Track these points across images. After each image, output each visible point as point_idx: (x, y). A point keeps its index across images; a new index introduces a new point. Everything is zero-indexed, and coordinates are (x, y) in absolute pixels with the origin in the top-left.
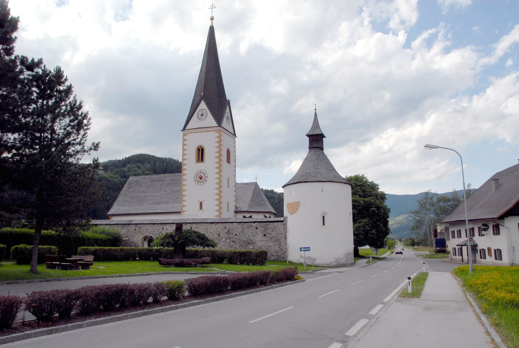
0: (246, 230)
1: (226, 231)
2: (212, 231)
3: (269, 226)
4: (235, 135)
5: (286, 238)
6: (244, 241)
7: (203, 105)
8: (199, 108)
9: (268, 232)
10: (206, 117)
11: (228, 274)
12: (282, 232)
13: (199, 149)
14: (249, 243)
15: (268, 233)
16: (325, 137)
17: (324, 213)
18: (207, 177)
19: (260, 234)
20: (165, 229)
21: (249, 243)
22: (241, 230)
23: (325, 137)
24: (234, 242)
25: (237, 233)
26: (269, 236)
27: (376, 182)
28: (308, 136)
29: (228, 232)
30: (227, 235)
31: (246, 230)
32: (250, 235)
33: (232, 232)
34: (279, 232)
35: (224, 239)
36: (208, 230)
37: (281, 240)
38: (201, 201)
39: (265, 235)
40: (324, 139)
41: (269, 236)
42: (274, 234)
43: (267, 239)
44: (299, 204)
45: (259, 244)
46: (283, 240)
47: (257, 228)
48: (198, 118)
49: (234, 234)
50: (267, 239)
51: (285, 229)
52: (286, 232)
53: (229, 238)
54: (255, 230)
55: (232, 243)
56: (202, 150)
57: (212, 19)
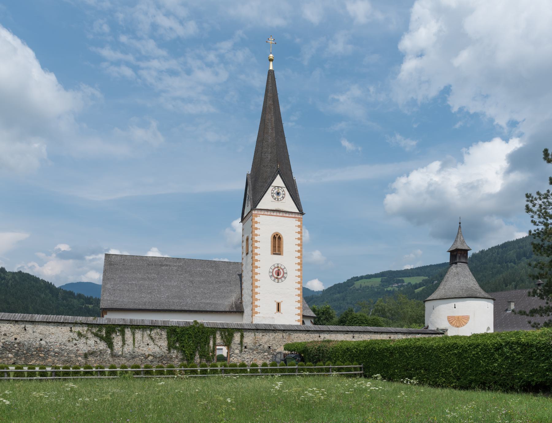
10: (283, 197)
13: (274, 237)
38: (279, 301)
48: (273, 196)
56: (280, 238)
57: (460, 223)
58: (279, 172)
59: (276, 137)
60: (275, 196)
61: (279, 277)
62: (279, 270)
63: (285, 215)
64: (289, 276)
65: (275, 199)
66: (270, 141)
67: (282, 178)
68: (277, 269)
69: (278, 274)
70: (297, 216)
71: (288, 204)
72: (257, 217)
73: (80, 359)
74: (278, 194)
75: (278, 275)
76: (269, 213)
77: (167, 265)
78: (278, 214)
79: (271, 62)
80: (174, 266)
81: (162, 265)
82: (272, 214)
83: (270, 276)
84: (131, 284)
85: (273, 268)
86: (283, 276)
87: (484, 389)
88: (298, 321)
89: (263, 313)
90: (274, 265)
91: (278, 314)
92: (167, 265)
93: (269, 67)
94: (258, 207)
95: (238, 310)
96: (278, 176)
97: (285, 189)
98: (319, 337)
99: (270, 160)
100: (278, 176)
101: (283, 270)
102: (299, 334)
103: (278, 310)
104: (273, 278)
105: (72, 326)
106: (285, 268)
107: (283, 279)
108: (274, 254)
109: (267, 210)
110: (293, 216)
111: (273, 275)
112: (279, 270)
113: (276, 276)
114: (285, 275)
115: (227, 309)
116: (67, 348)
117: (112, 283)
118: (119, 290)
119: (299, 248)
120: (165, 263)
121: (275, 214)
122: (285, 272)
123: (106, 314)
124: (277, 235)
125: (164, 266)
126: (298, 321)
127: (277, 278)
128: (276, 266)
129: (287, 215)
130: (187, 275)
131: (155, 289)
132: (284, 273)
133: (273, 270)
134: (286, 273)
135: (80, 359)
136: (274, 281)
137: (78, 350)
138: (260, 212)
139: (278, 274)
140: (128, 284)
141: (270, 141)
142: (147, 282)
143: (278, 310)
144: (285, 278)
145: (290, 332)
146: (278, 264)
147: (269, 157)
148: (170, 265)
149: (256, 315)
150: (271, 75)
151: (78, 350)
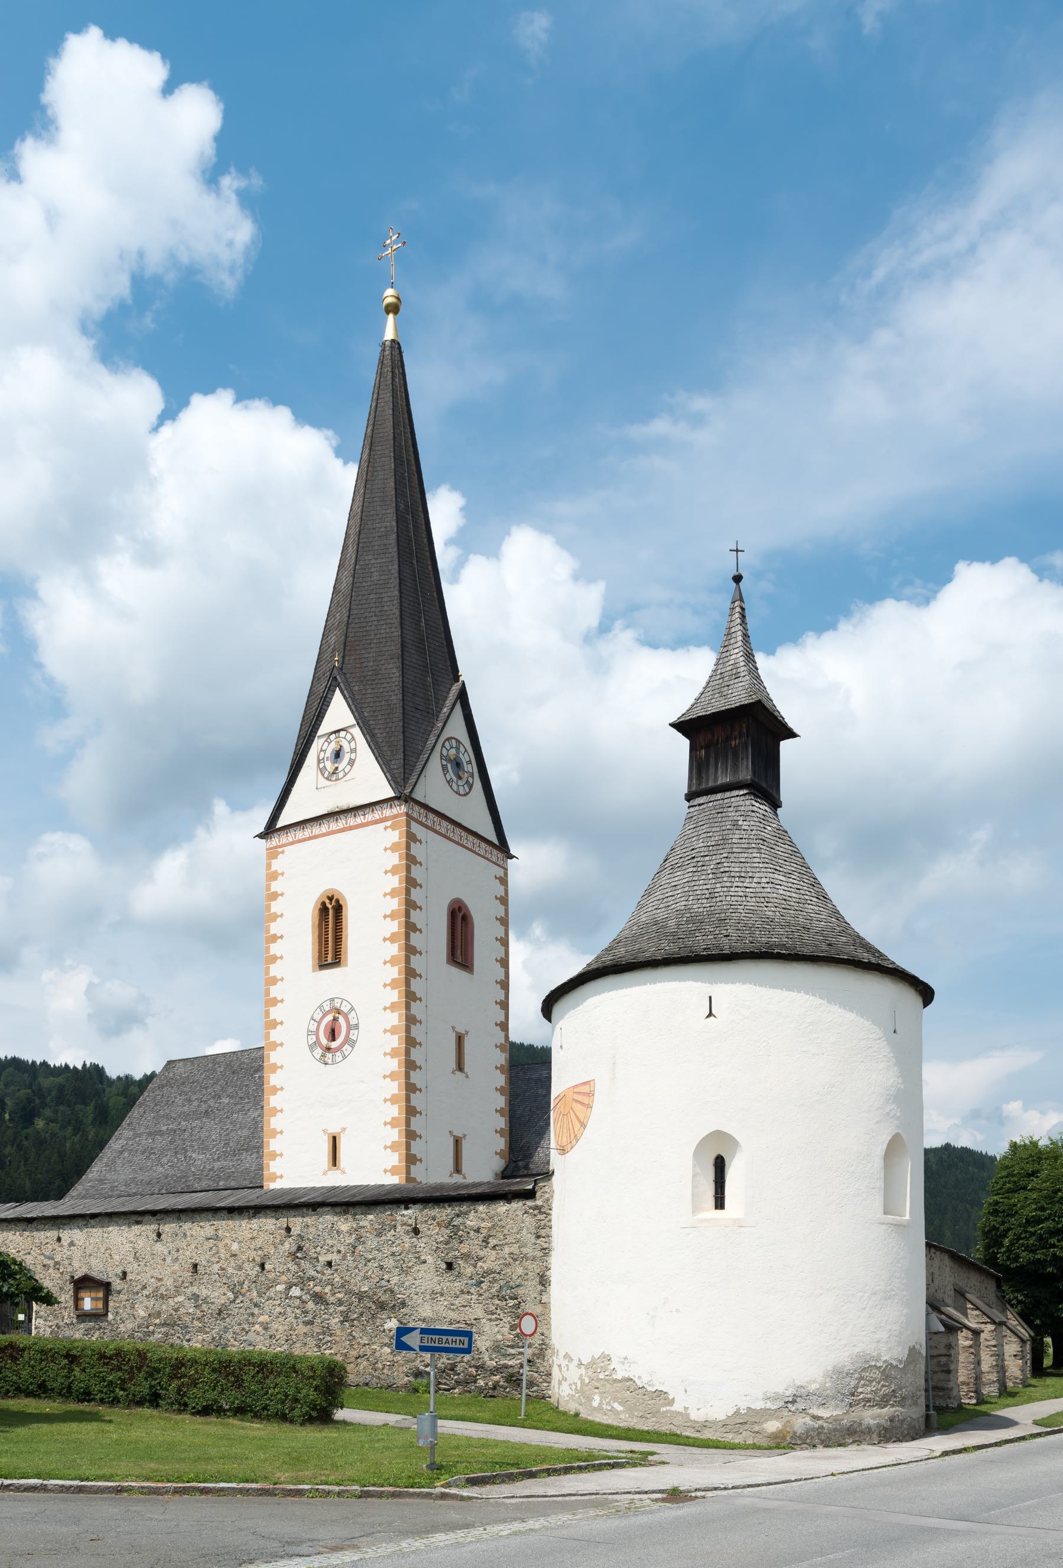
0: (372, 1242)
1: (289, 1245)
2: (235, 1247)
3: (472, 1221)
4: (502, 847)
5: (544, 1281)
6: (361, 1296)
7: (339, 712)
8: (325, 727)
9: (464, 1248)
10: (352, 762)
11: (826, 1420)
12: (528, 1251)
13: (323, 910)
14: (382, 1306)
15: (466, 1257)
16: (791, 734)
17: (719, 1136)
18: (357, 1026)
19: (430, 1259)
20: (65, 1242)
21: (382, 1306)
22: (351, 1240)
23: (791, 734)
24: (319, 1298)
25: (334, 1257)
26: (469, 1270)
27: (783, 804)
28: (682, 726)
29: (298, 1253)
30: (294, 1268)
31: (372, 1242)
32: (389, 1263)
33: (312, 1253)
34: (515, 1249)
35: (280, 1288)
36: (221, 1245)
37: (521, 1295)
38: (334, 1129)
39: (450, 1266)
40: (785, 746)
41: (469, 1270)
42: (491, 1260)
43: (458, 1285)
44: (590, 1094)
45: (426, 1311)
46: (529, 1290)
47: (416, 1231)
48: (322, 771)
49: (323, 1259)
50: (458, 1285)
51: (543, 1232)
52: (546, 1251)
53: (302, 1281)
54: (408, 1241)
55: (311, 1305)
56: (339, 909)
57: (738, 579)
61: (334, 1045)
62: (335, 1019)
70: (388, 812)
74: (337, 755)
75: (334, 1039)
78: (334, 826)
79: (391, 316)
88: (394, 1171)
93: (383, 333)
94: (280, 824)
96: (338, 690)
97: (357, 732)
98: (59, 1239)
100: (338, 690)
107: (347, 1048)
111: (318, 1042)
112: (335, 1019)
113: (324, 1041)
121: (324, 828)
122: (353, 1022)
124: (331, 899)
126: (394, 1171)
128: (327, 1009)
129: (360, 819)
133: (319, 1023)
139: (334, 1033)
150: (394, 361)
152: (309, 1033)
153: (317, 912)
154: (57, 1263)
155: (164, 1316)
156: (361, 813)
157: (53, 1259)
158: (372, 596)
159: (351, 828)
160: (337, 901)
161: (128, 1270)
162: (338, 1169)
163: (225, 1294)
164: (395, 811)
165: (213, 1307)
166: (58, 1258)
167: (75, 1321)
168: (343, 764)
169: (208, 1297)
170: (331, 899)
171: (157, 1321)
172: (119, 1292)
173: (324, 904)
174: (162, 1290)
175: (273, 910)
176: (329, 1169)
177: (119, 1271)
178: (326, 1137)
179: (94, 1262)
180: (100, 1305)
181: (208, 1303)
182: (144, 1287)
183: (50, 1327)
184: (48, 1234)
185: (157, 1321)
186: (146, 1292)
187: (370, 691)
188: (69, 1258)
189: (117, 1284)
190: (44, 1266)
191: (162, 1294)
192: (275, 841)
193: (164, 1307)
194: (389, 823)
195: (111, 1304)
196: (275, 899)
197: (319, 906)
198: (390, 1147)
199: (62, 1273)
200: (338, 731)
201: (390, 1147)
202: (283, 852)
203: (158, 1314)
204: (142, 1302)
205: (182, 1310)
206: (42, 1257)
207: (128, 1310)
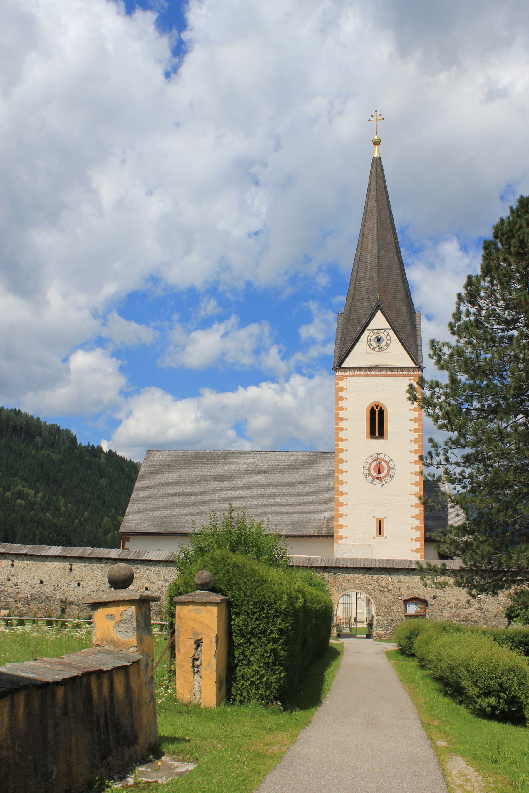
10: (388, 345)
38: (380, 517)
48: (370, 345)
56: (382, 413)
58: (379, 306)
59: (379, 253)
60: (374, 344)
61: (382, 475)
63: (390, 373)
64: (397, 474)
65: (374, 349)
66: (369, 260)
67: (384, 315)
68: (375, 463)
69: (379, 470)
71: (396, 354)
72: (342, 380)
73: (19, 605)
74: (379, 340)
75: (379, 473)
76: (362, 373)
77: (232, 463)
78: (379, 373)
80: (245, 463)
81: (225, 464)
82: (368, 373)
83: (366, 476)
84: (172, 495)
85: (370, 460)
86: (388, 474)
87: (412, 699)
89: (354, 543)
90: (371, 457)
91: (379, 538)
92: (232, 463)
93: (374, 154)
94: (344, 365)
95: (329, 536)
97: (391, 332)
99: (368, 289)
101: (387, 463)
102: (352, 575)
103: (380, 533)
104: (370, 478)
105: (13, 558)
106: (391, 460)
108: (372, 438)
109: (360, 368)
110: (405, 373)
111: (369, 473)
112: (380, 463)
113: (375, 474)
114: (392, 472)
115: (311, 533)
116: (5, 589)
117: (147, 493)
118: (153, 504)
119: (341, 424)
120: (231, 459)
121: (373, 373)
122: (392, 466)
123: (129, 541)
124: (377, 407)
125: (228, 464)
127: (377, 478)
130: (260, 477)
131: (206, 502)
132: (389, 469)
133: (370, 464)
134: (394, 469)
135: (19, 605)
136: (372, 482)
137: (18, 593)
138: (347, 373)
139: (379, 470)
140: (168, 495)
141: (369, 260)
142: (196, 491)
143: (380, 533)
144: (392, 477)
145: (336, 571)
146: (379, 454)
147: (367, 285)
148: (237, 463)
149: (340, 542)
151: (18, 593)
152: (364, 468)
153: (369, 411)
154: (389, 590)
155: (461, 617)
156: (395, 370)
157: (386, 588)
158: (388, 270)
159: (389, 376)
160: (381, 408)
161: (438, 596)
162: (383, 536)
163: (498, 608)
164: (416, 373)
165: (491, 613)
166: (390, 587)
167: (404, 618)
168: (383, 344)
169: (488, 609)
170: (377, 407)
171: (458, 619)
172: (433, 605)
173: (373, 408)
174: (460, 605)
175: (340, 406)
176: (377, 536)
177: (432, 595)
178: (375, 520)
179: (414, 590)
180: (423, 610)
181: (488, 612)
182: (449, 603)
183: (387, 620)
184: (383, 576)
185: (458, 619)
186: (449, 606)
187: (394, 314)
188: (399, 588)
189: (430, 601)
190: (381, 591)
191: (460, 607)
192: (341, 373)
193: (462, 613)
194: (412, 378)
195: (428, 610)
196: (342, 400)
197: (370, 409)
198: (415, 528)
199: (394, 595)
200: (380, 329)
201: (415, 528)
202: (347, 379)
203: (459, 616)
204: (448, 610)
205: (473, 615)
206: (379, 587)
207: (439, 613)
